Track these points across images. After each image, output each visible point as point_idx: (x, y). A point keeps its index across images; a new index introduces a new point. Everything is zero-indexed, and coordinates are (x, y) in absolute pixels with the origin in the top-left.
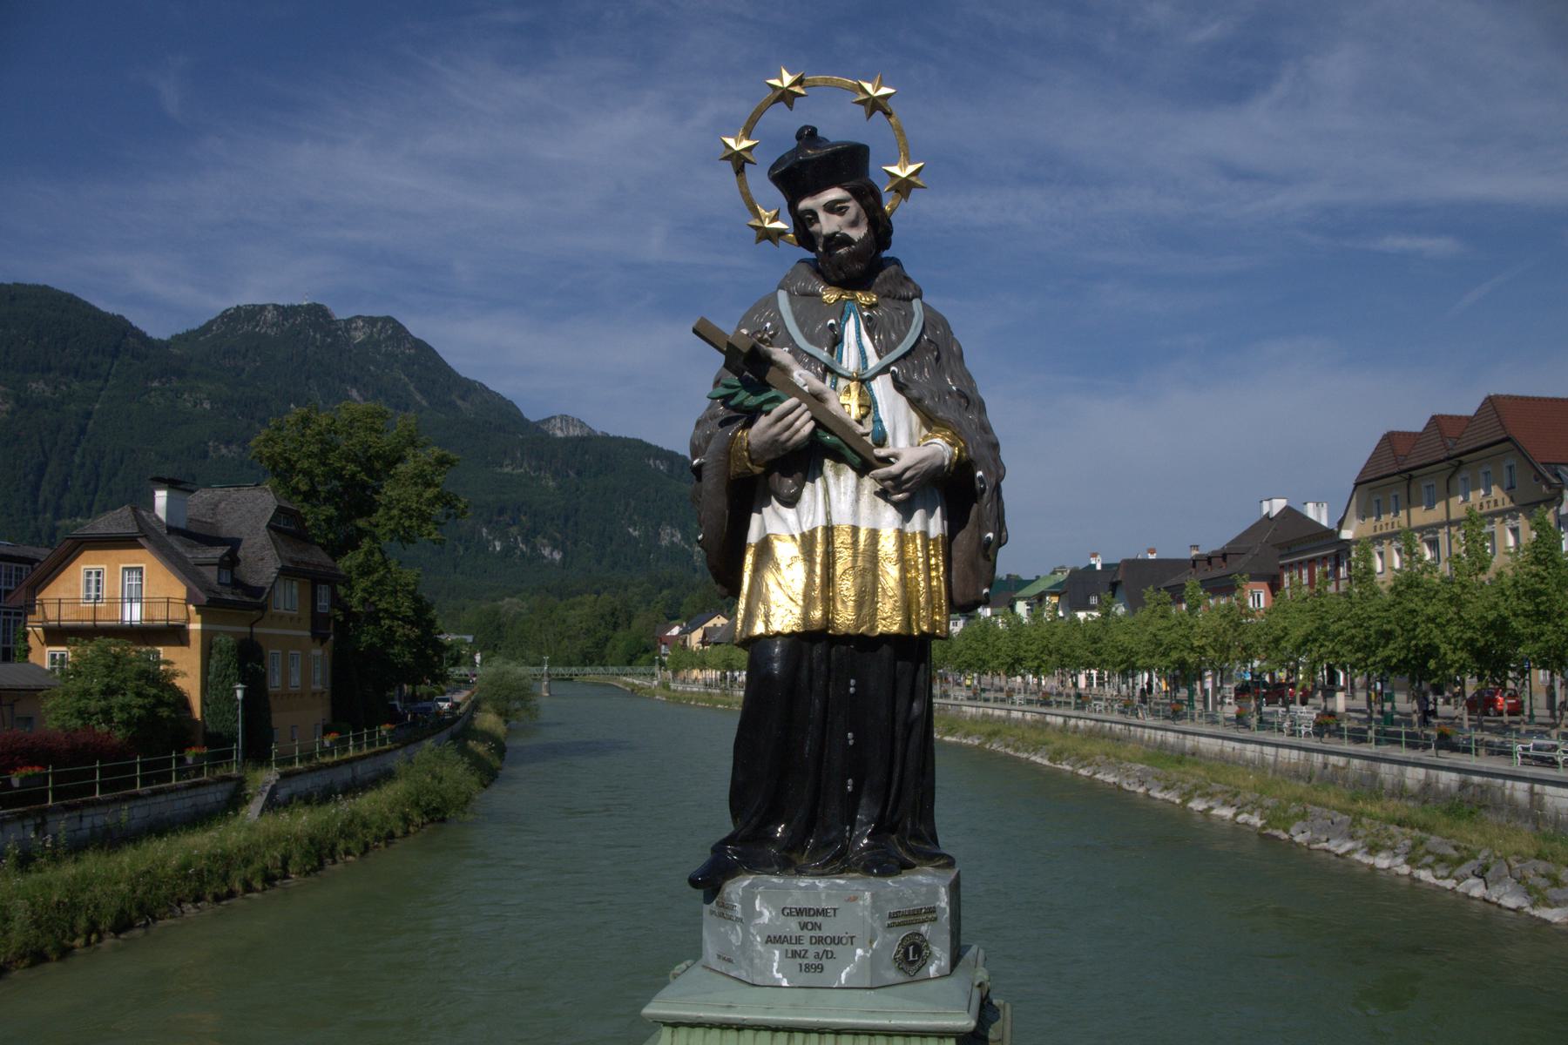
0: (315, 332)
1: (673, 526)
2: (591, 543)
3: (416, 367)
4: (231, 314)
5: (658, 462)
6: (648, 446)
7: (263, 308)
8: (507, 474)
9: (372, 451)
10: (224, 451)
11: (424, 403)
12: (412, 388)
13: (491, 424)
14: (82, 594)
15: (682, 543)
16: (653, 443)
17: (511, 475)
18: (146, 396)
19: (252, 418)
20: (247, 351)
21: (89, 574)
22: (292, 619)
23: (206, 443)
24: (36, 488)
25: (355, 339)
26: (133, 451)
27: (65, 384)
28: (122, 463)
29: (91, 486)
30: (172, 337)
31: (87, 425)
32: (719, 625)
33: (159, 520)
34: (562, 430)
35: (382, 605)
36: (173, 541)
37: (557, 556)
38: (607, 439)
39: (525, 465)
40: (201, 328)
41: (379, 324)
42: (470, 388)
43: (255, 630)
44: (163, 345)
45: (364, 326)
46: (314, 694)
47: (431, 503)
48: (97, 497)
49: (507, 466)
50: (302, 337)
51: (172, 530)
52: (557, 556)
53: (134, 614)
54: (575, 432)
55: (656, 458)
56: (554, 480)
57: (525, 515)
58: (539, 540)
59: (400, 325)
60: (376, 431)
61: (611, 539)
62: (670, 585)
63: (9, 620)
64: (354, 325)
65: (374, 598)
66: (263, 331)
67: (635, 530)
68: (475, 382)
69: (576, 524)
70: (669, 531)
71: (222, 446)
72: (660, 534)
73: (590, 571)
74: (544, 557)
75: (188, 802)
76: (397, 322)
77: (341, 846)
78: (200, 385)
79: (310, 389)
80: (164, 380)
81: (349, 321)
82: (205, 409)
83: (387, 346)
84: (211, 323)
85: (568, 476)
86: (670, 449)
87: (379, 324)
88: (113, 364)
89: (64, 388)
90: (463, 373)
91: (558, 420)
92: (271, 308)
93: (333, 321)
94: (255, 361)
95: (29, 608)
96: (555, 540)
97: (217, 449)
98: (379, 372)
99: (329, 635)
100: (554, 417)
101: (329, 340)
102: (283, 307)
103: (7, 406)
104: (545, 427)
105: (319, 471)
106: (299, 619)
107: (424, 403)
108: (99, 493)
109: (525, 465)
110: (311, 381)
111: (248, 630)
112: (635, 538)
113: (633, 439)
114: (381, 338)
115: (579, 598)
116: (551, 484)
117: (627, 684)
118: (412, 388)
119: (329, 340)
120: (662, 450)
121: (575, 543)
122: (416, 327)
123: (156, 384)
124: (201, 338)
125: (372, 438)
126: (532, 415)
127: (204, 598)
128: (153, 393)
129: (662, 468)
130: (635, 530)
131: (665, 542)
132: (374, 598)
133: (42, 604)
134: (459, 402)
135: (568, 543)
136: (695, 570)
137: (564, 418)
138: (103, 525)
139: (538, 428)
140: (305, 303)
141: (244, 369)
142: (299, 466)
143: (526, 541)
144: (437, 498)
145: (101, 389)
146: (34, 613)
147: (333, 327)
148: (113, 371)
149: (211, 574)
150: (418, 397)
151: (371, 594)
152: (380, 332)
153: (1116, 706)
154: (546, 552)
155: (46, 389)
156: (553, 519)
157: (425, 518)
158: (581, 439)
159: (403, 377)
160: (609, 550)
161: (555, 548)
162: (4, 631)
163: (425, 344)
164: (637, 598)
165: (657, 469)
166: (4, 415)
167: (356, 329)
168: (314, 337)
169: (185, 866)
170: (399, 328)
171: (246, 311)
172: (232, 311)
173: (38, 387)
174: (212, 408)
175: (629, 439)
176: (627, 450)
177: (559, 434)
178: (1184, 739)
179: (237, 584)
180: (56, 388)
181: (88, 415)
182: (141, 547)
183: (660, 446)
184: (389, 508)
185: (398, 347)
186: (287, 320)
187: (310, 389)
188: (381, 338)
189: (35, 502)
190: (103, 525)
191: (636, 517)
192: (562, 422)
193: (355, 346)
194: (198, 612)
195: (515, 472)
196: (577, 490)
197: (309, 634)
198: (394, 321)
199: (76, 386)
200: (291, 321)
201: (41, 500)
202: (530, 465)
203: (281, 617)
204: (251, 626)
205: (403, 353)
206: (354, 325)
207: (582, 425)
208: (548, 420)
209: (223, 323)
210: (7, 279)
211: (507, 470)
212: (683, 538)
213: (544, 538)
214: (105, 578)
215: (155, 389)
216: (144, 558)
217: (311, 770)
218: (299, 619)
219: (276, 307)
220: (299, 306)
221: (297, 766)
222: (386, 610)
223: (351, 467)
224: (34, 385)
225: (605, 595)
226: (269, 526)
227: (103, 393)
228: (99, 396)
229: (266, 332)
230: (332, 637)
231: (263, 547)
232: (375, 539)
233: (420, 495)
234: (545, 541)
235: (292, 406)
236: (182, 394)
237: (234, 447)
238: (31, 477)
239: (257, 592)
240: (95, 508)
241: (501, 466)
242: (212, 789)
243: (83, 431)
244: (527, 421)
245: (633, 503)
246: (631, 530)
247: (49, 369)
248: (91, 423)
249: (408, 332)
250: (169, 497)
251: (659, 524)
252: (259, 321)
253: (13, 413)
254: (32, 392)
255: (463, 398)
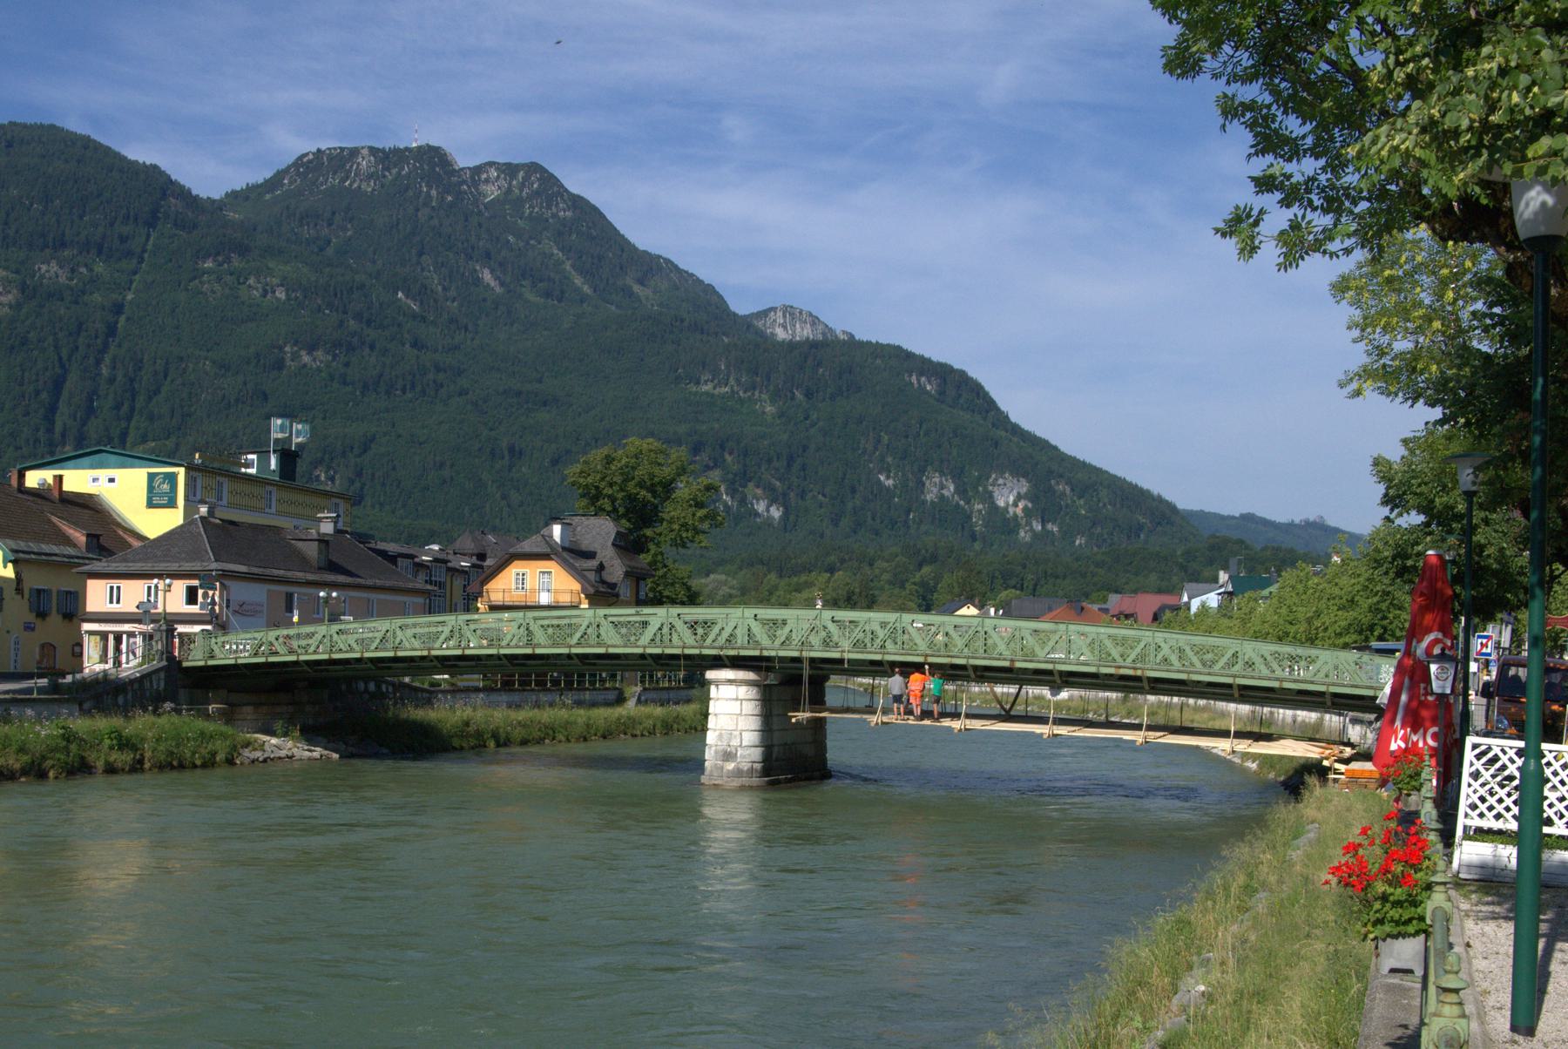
0: (430, 187)
1: (942, 474)
2: (824, 495)
3: (574, 237)
4: (310, 161)
5: (923, 379)
6: (909, 356)
7: (354, 152)
8: (707, 393)
9: (656, 479)
10: (306, 359)
11: (586, 289)
12: (568, 266)
13: (682, 321)
14: (513, 587)
15: (956, 497)
16: (918, 351)
17: (713, 395)
18: (197, 281)
19: (345, 312)
20: (334, 213)
21: (518, 574)
23: (281, 348)
24: (52, 409)
25: (485, 196)
26: (181, 359)
27: (86, 265)
28: (166, 376)
29: (126, 408)
30: (227, 194)
31: (117, 322)
33: (556, 543)
34: (785, 327)
35: (666, 593)
36: (565, 554)
37: (776, 513)
38: (852, 345)
39: (732, 381)
40: (266, 181)
41: (521, 174)
42: (652, 266)
44: (221, 200)
45: (498, 177)
47: (702, 520)
48: (133, 423)
49: (706, 382)
50: (410, 193)
51: (564, 549)
52: (776, 513)
53: (545, 599)
54: (804, 332)
55: (921, 374)
56: (773, 401)
57: (730, 454)
58: (751, 490)
59: (552, 176)
60: (659, 464)
61: (853, 491)
62: (933, 559)
64: (484, 176)
65: (660, 588)
66: (355, 185)
67: (888, 477)
68: (660, 257)
69: (804, 468)
70: (937, 480)
71: (303, 353)
72: (924, 485)
73: (822, 536)
74: (757, 514)
76: (547, 171)
77: (675, 726)
78: (270, 265)
79: (423, 270)
80: (220, 259)
81: (478, 170)
82: (278, 299)
83: (532, 207)
84: (280, 175)
85: (793, 398)
86: (942, 360)
87: (521, 174)
88: (148, 236)
89: (83, 270)
90: (641, 246)
91: (780, 314)
92: (365, 152)
93: (455, 170)
94: (345, 229)
95: (480, 594)
96: (772, 489)
97: (295, 356)
98: (521, 244)
100: (773, 309)
101: (450, 198)
102: (383, 151)
103: (10, 297)
104: (760, 324)
105: (620, 495)
107: (586, 289)
108: (136, 418)
109: (732, 381)
110: (424, 257)
112: (888, 489)
113: (888, 345)
114: (524, 194)
115: (803, 578)
116: (768, 409)
117: (861, 685)
118: (568, 266)
119: (450, 198)
120: (929, 361)
121: (802, 495)
122: (576, 182)
123: (209, 264)
124: (268, 197)
125: (656, 471)
126: (741, 306)
127: (592, 591)
128: (205, 277)
129: (929, 388)
130: (888, 477)
131: (930, 496)
132: (660, 588)
133: (488, 592)
134: (637, 288)
135: (792, 495)
136: (974, 538)
137: (788, 311)
138: (527, 546)
139: (749, 326)
140: (414, 145)
141: (329, 242)
142: (605, 492)
143: (732, 492)
144: (706, 517)
145: (135, 273)
146: (482, 596)
147: (454, 179)
148: (149, 247)
149: (592, 576)
150: (578, 281)
151: (658, 585)
152: (522, 186)
154: (761, 507)
155: (60, 272)
156: (770, 461)
157: (697, 531)
158: (812, 345)
159: (556, 252)
160: (850, 505)
161: (773, 502)
164: (886, 577)
165: (922, 389)
166: (6, 309)
167: (487, 181)
168: (428, 194)
169: (619, 719)
170: (549, 180)
171: (331, 157)
172: (311, 157)
173: (50, 270)
174: (288, 298)
175: (882, 346)
176: (878, 361)
177: (781, 334)
179: (603, 582)
180: (73, 270)
181: (118, 309)
182: (551, 559)
183: (927, 355)
184: (671, 522)
185: (549, 207)
186: (388, 169)
187: (423, 270)
188: (524, 194)
189: (50, 430)
190: (527, 546)
191: (889, 459)
192: (784, 316)
193: (487, 206)
194: (586, 598)
195: (716, 392)
196: (806, 419)
198: (543, 170)
199: (100, 268)
200: (394, 171)
201: (58, 428)
202: (738, 381)
205: (554, 216)
206: (484, 176)
207: (815, 320)
208: (764, 314)
209: (298, 174)
210: (2, 119)
211: (705, 388)
212: (957, 491)
213: (758, 487)
214: (528, 578)
215: (208, 272)
216: (552, 566)
217: (654, 689)
219: (373, 151)
220: (407, 149)
222: (668, 597)
223: (643, 493)
224: (44, 268)
225: (839, 575)
226: (613, 544)
227: (137, 277)
228: (131, 282)
229: (359, 187)
231: (612, 558)
232: (658, 545)
233: (694, 515)
234: (759, 491)
235: (400, 295)
236: (247, 279)
237: (319, 354)
238: (44, 395)
239: (613, 586)
240: (130, 440)
241: (698, 383)
242: (610, 692)
243: (112, 330)
244: (735, 314)
245: (885, 439)
246: (882, 478)
247: (63, 245)
248: (122, 319)
249: (563, 186)
250: (562, 529)
251: (922, 471)
252: (350, 171)
253: (17, 307)
254: (42, 277)
255: (641, 282)
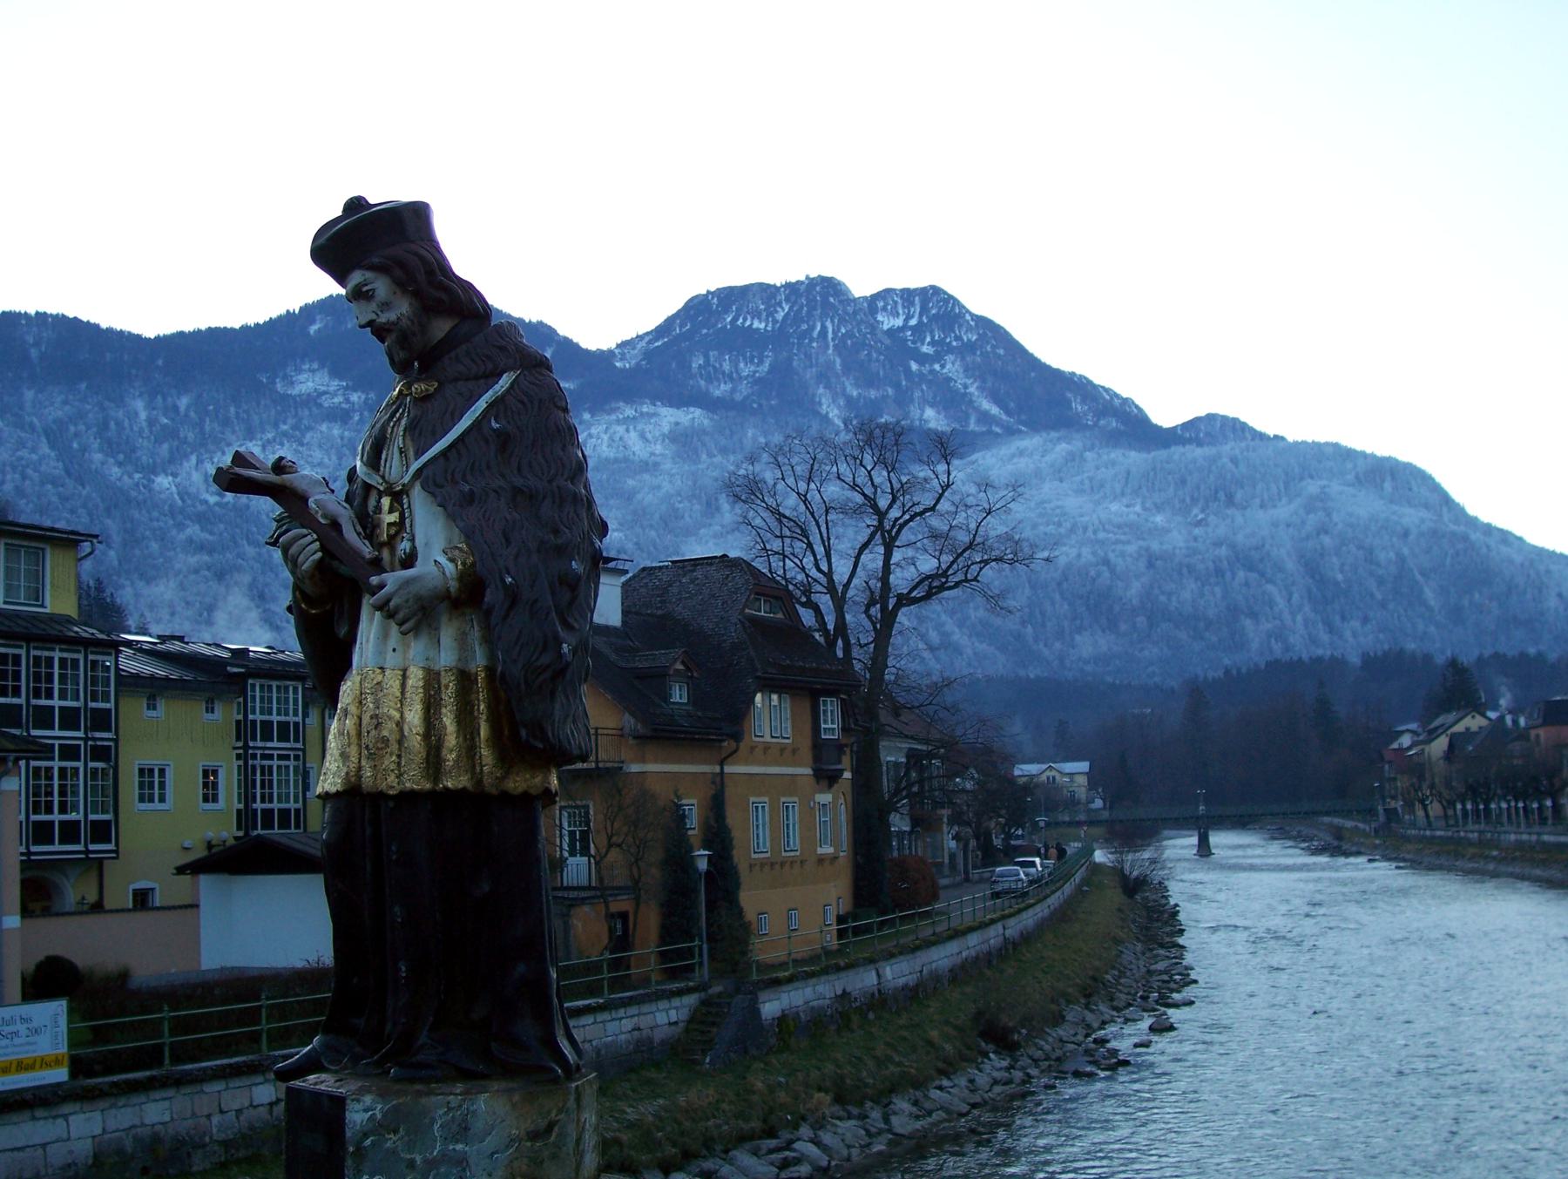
22: (783, 749)
32: (1474, 728)
43: (727, 769)
44: (604, 357)
46: (821, 860)
63: (287, 767)
66: (748, 323)
75: (628, 1024)
99: (842, 771)
106: (794, 751)
111: (717, 769)
153: (1018, 369)
162: (205, 785)
163: (1006, 333)
178: (864, 568)
197: (809, 771)
203: (767, 747)
204: (722, 764)
218: (794, 751)
221: (167, 1013)
230: (847, 775)
